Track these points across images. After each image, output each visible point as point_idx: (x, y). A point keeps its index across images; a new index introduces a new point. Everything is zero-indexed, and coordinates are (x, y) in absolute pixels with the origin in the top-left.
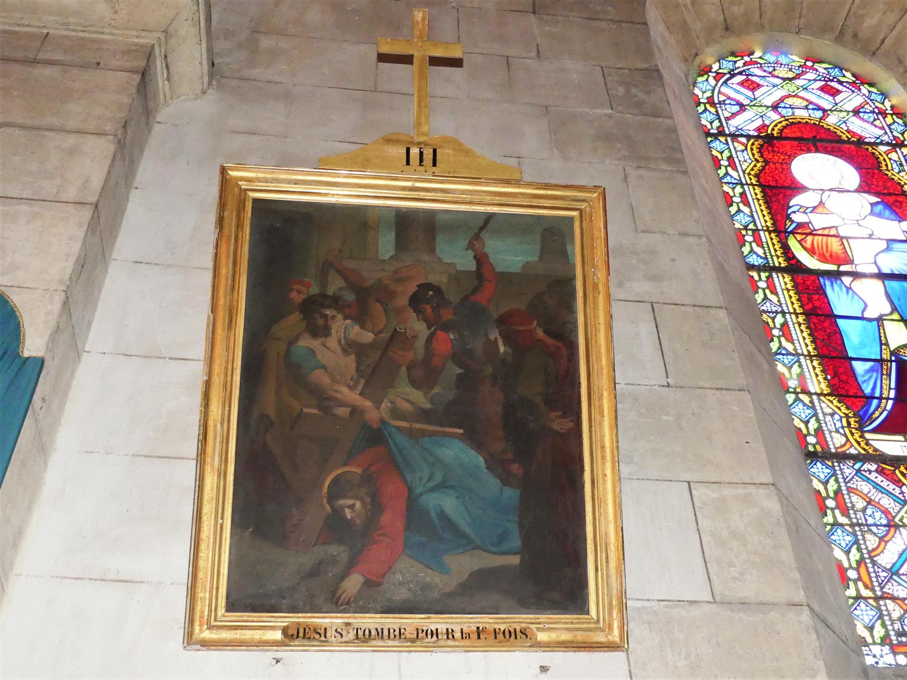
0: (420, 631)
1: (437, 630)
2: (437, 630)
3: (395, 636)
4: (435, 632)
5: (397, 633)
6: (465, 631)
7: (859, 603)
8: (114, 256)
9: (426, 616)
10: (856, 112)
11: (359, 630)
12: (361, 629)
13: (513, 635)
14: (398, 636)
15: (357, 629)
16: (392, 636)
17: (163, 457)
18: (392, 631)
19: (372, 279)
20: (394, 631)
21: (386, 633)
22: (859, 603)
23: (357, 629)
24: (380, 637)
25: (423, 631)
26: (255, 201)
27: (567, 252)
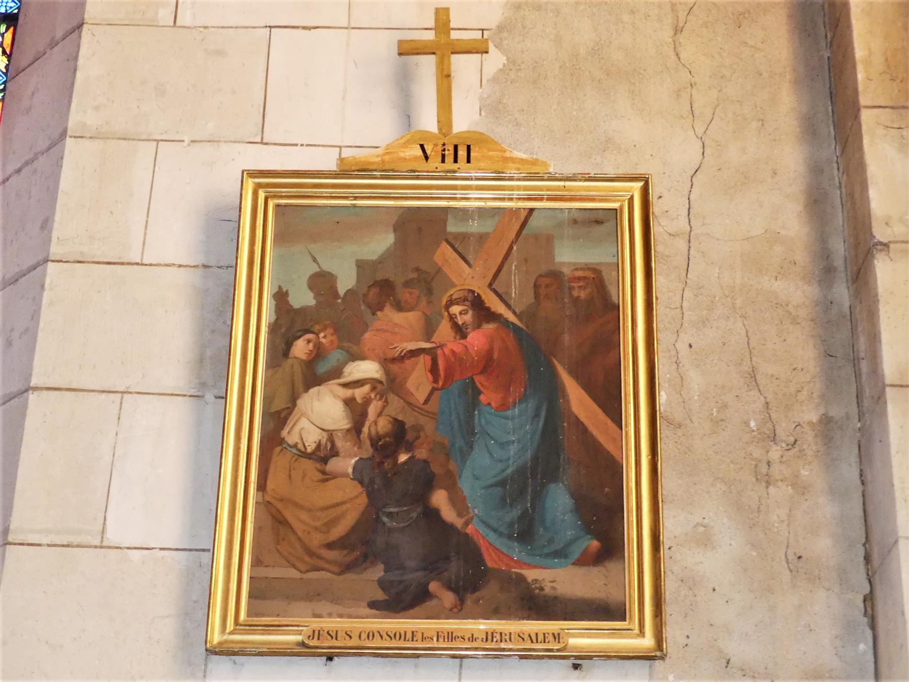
5: (507, 637)
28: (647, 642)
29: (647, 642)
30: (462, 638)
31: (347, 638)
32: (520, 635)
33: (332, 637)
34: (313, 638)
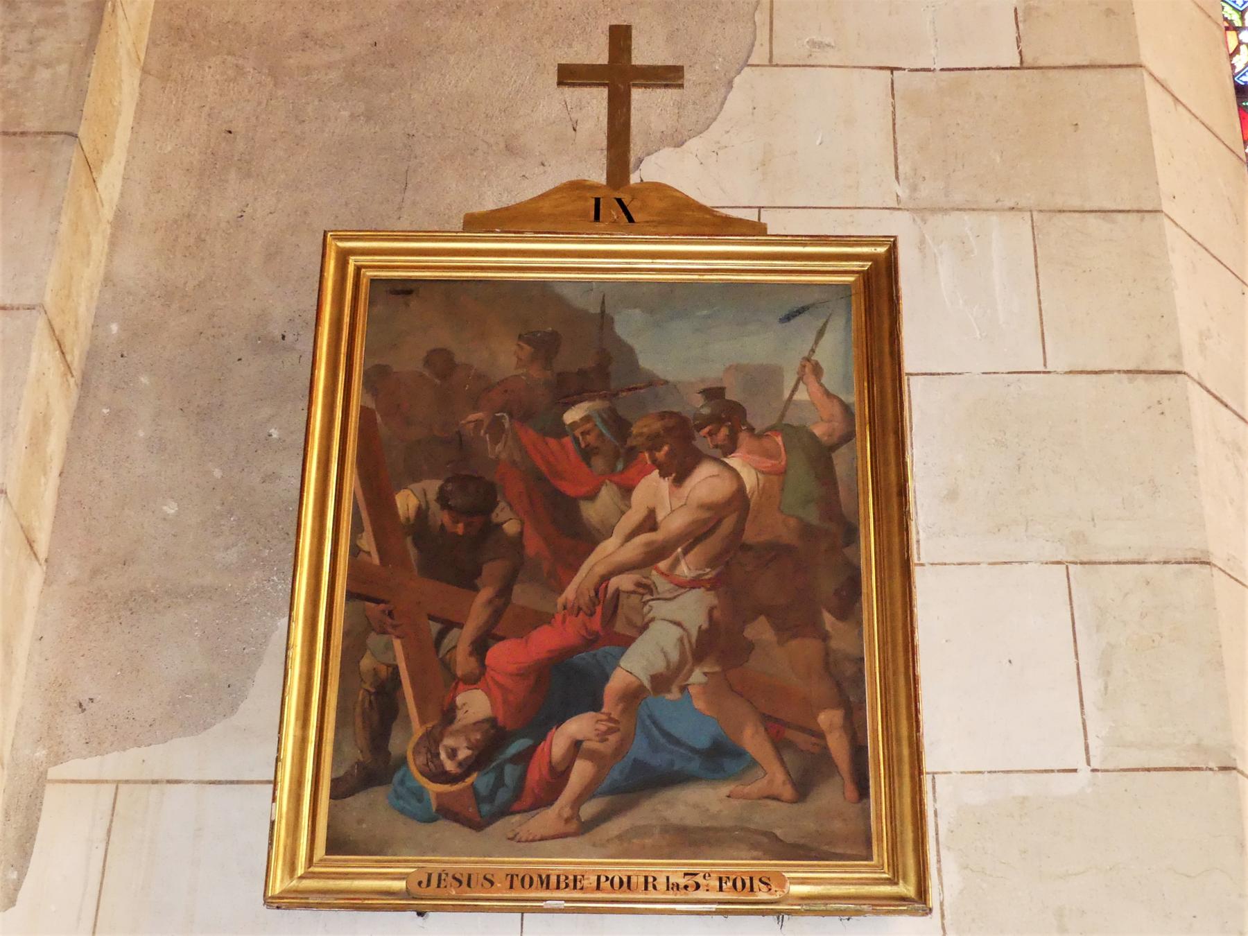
0: (603, 879)
1: (629, 878)
2: (629, 878)
3: (567, 885)
4: (625, 880)
6: (671, 881)
7: (1243, 5)
8: (714, 916)
9: (651, 261)
10: (326, 74)
11: (515, 877)
12: (517, 875)
13: (625, 885)
14: (571, 884)
15: (512, 876)
16: (563, 885)
17: (1215, 257)
18: (562, 878)
19: (538, 332)
20: (567, 878)
21: (553, 880)
22: (1243, 5)
23: (512, 876)
24: (545, 885)
25: (607, 879)
26: (373, 281)
27: (373, 531)
28: (907, 888)
29: (907, 888)
30: (454, 878)
31: (487, 884)
32: (488, 877)
33: (460, 882)
34: (428, 885)
